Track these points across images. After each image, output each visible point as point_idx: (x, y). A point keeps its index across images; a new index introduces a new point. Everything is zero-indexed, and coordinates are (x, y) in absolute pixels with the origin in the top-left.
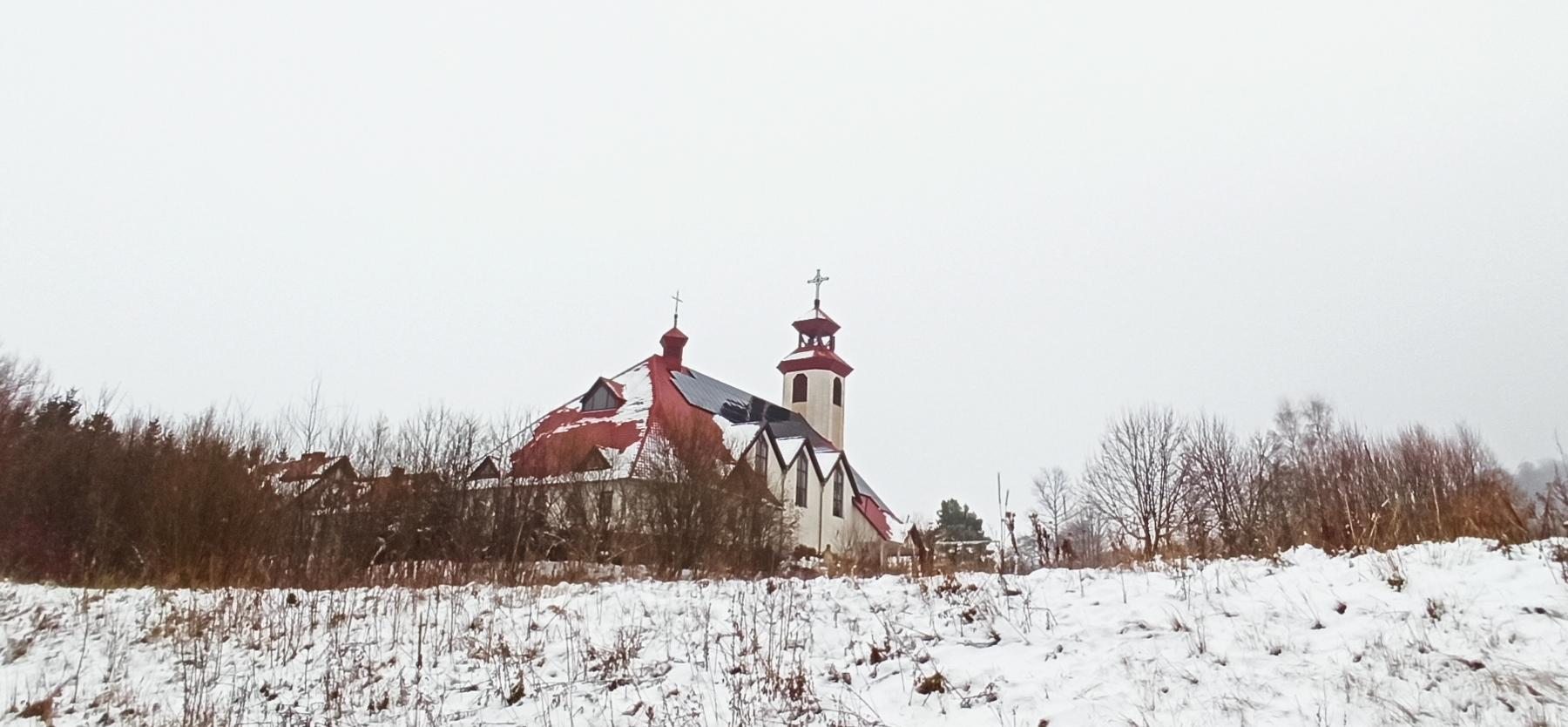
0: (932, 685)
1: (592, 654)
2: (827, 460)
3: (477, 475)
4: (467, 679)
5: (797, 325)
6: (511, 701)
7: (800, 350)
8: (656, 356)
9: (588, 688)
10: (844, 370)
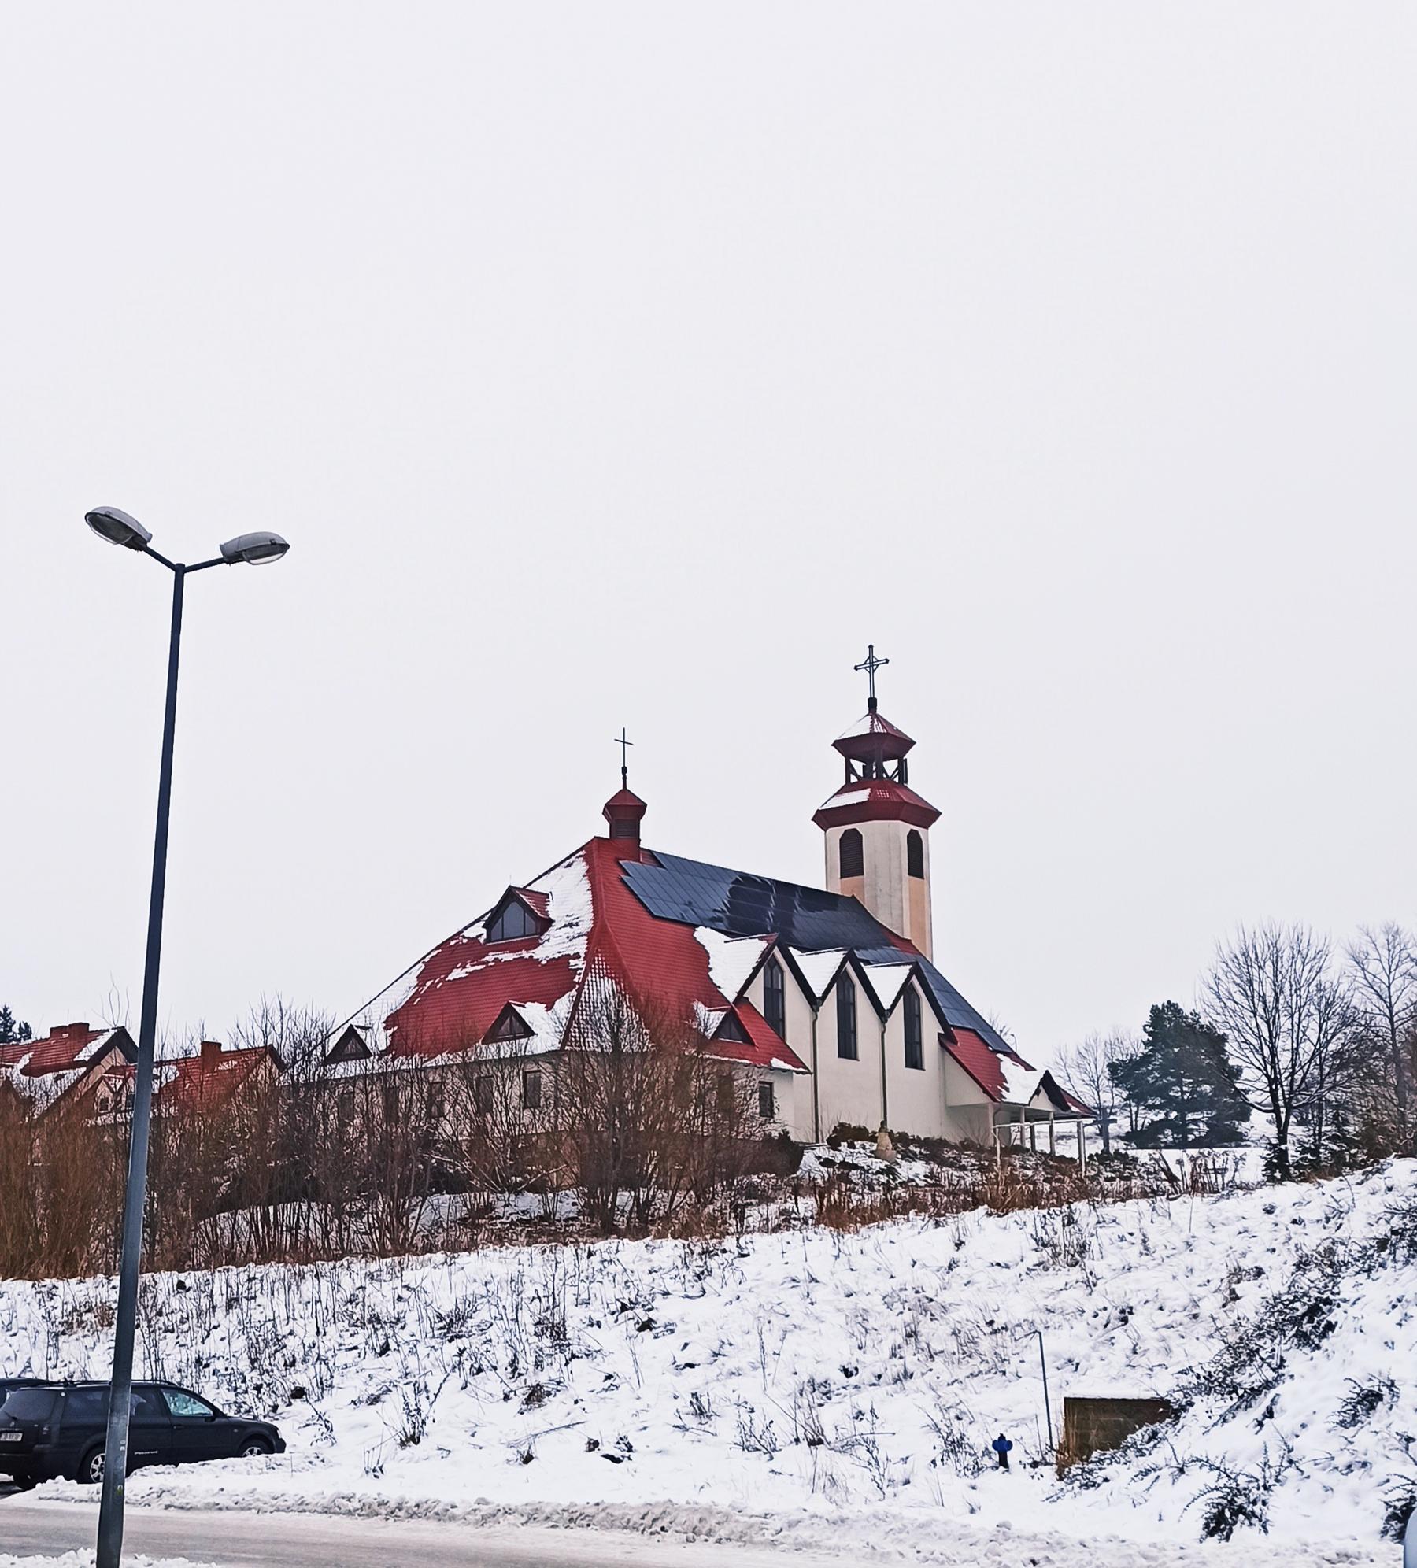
0: (647, 1326)
1: (440, 1317)
2: (887, 980)
3: (339, 1054)
4: (349, 1342)
5: (841, 745)
6: (381, 1354)
7: (848, 788)
8: (598, 839)
9: (433, 1342)
10: (927, 815)
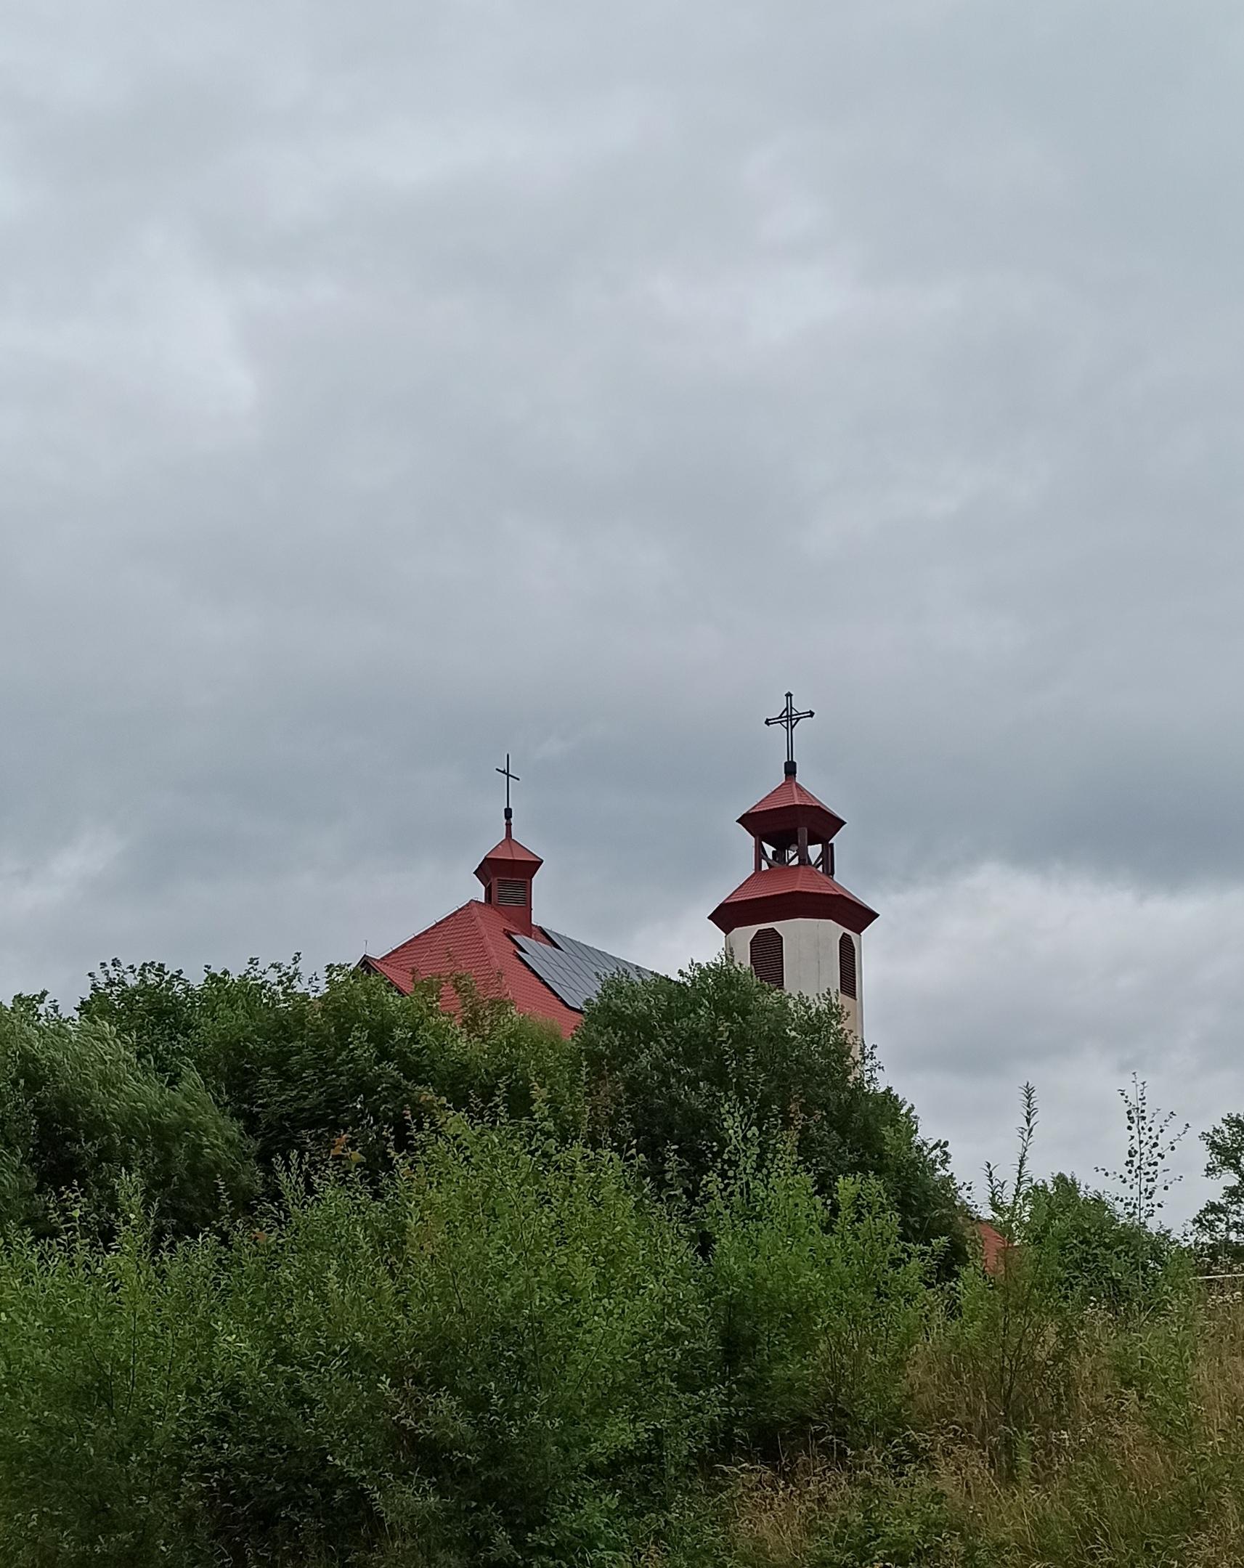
8: (473, 903)
10: (858, 916)
